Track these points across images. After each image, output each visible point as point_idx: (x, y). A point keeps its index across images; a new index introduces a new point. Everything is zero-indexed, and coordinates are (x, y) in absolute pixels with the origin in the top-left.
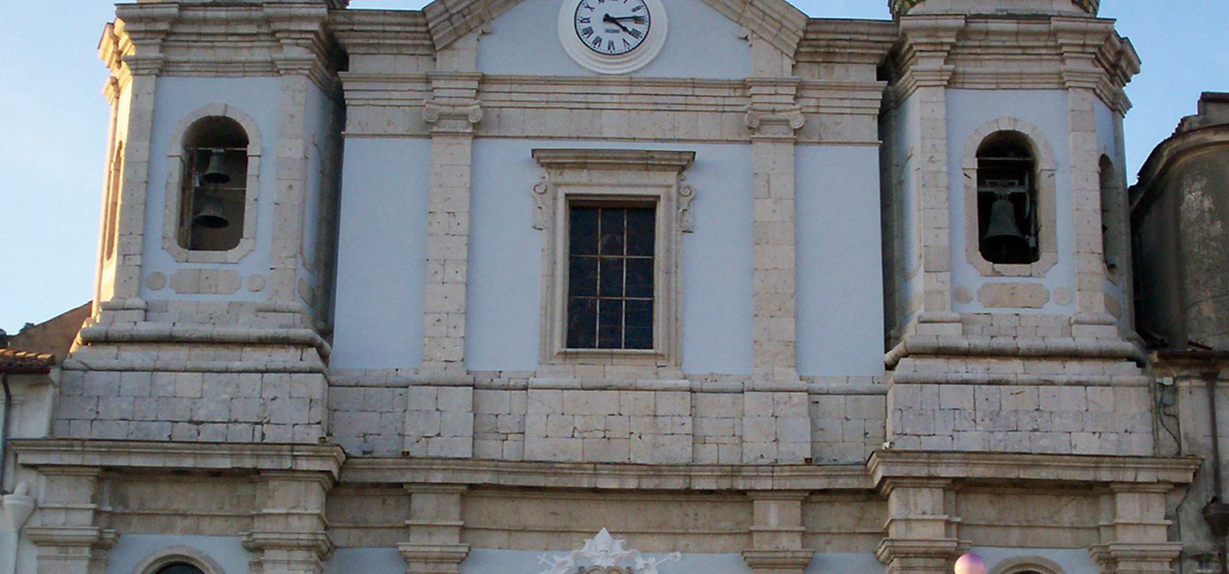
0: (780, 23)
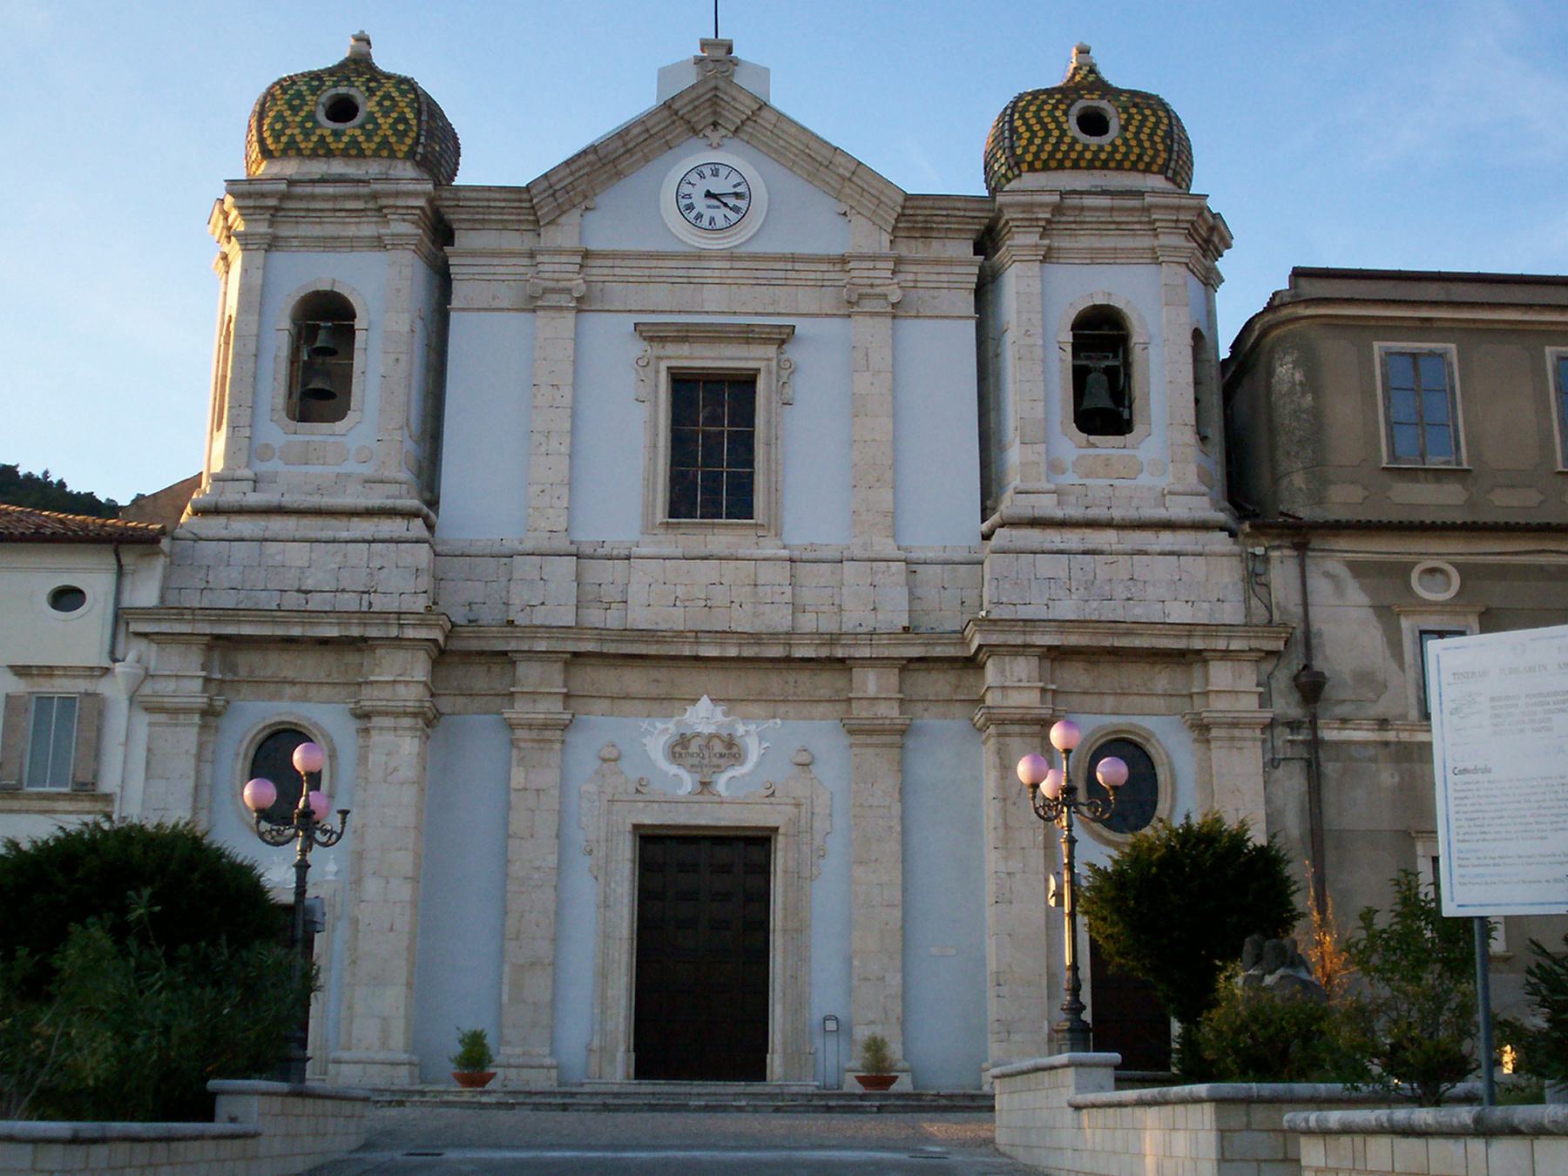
0: (879, 199)
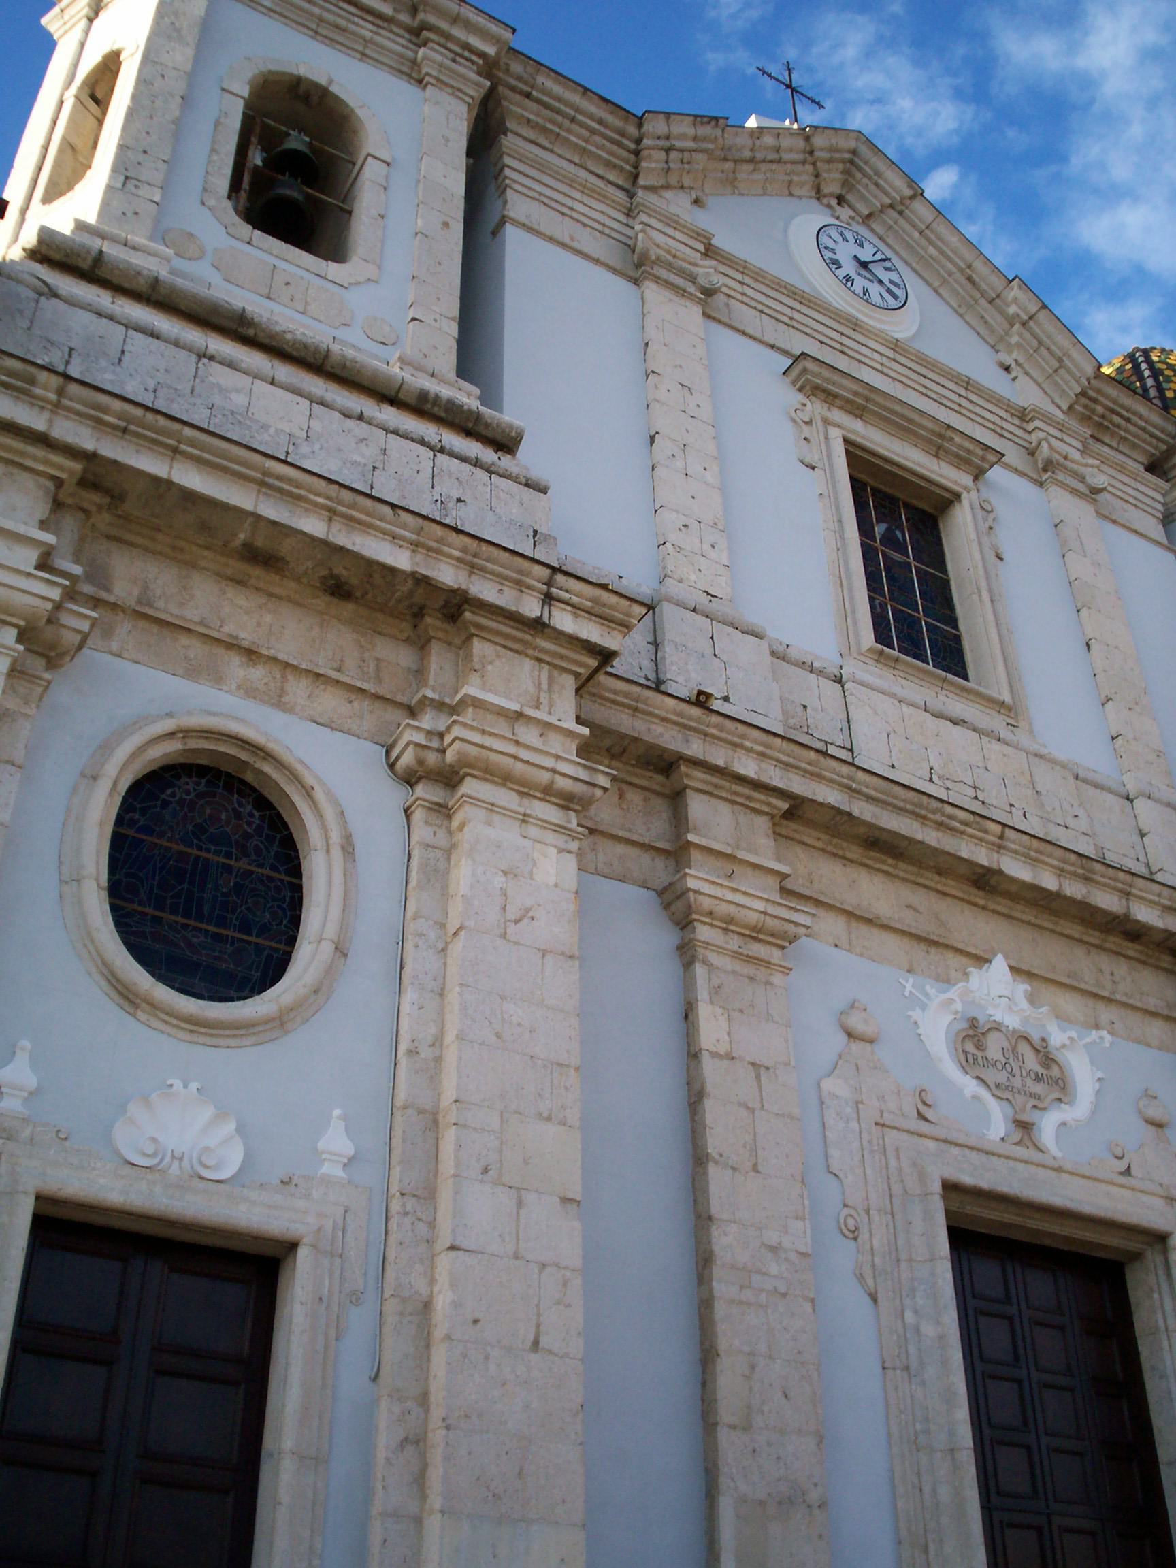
0: (1060, 360)
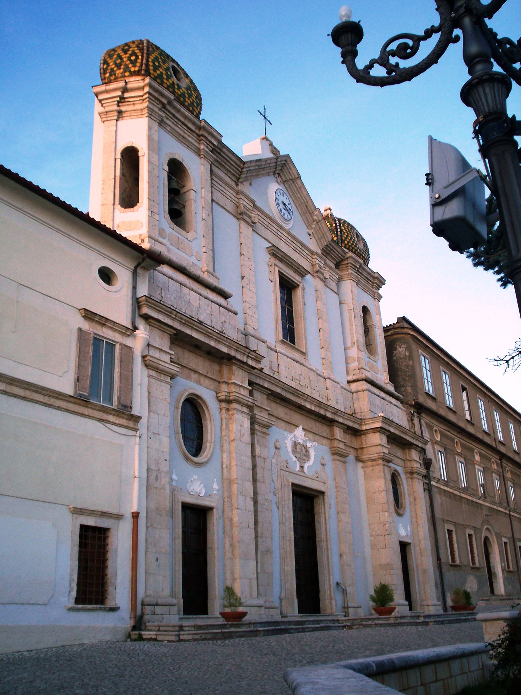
0: (323, 235)
